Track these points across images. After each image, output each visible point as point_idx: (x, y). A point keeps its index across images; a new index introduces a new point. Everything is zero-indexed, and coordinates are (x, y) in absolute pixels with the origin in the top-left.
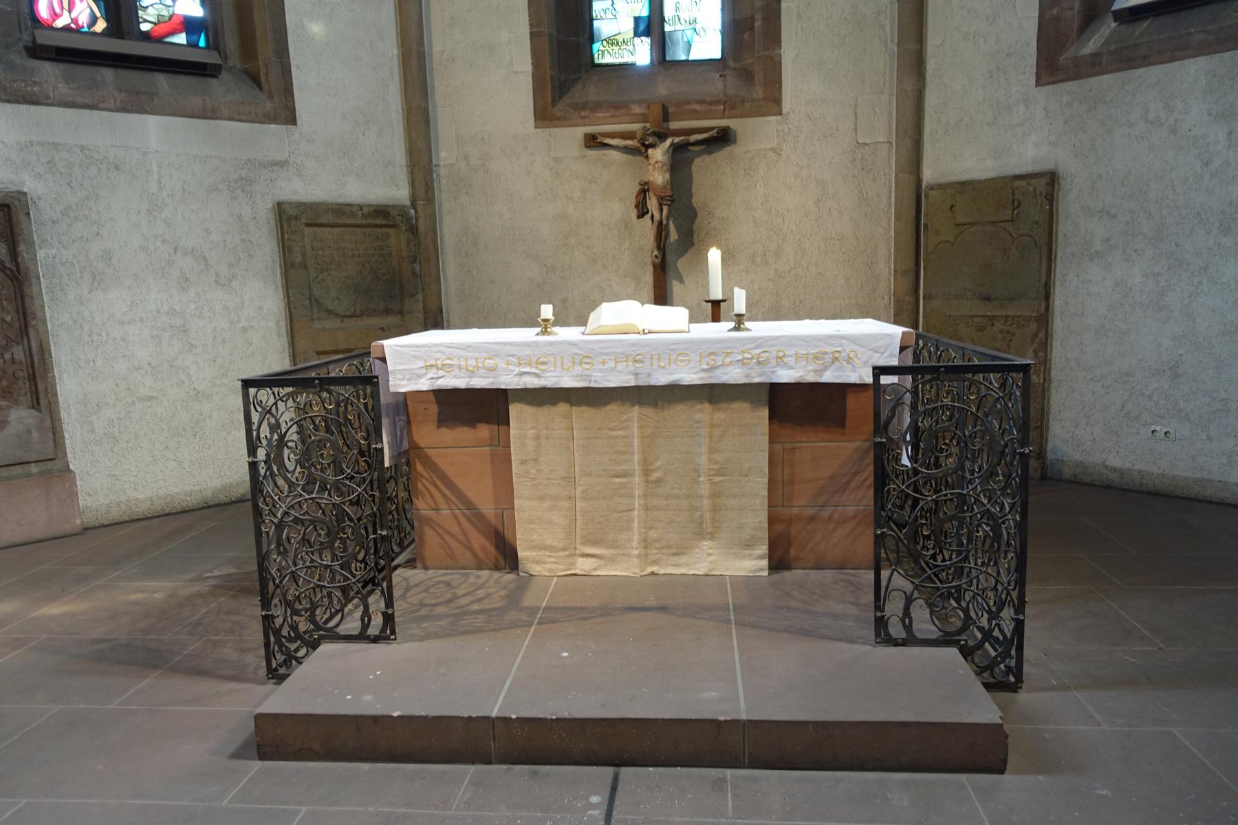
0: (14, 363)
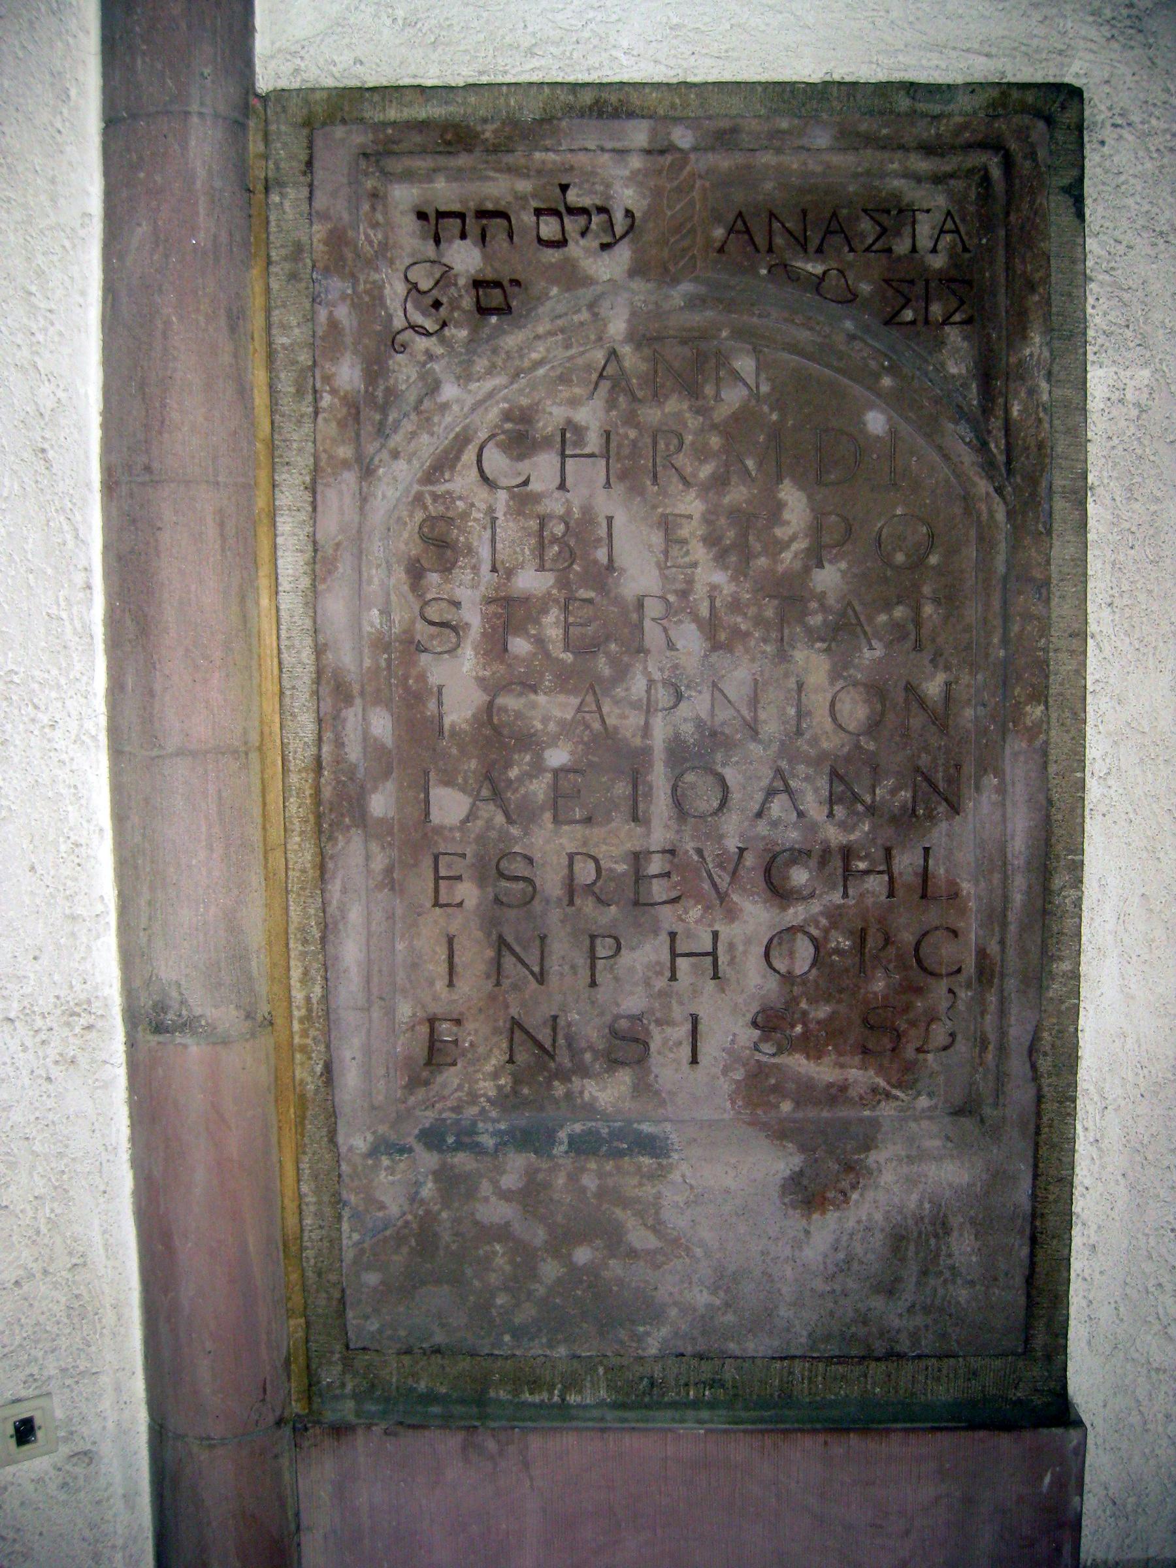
0: (924, 896)
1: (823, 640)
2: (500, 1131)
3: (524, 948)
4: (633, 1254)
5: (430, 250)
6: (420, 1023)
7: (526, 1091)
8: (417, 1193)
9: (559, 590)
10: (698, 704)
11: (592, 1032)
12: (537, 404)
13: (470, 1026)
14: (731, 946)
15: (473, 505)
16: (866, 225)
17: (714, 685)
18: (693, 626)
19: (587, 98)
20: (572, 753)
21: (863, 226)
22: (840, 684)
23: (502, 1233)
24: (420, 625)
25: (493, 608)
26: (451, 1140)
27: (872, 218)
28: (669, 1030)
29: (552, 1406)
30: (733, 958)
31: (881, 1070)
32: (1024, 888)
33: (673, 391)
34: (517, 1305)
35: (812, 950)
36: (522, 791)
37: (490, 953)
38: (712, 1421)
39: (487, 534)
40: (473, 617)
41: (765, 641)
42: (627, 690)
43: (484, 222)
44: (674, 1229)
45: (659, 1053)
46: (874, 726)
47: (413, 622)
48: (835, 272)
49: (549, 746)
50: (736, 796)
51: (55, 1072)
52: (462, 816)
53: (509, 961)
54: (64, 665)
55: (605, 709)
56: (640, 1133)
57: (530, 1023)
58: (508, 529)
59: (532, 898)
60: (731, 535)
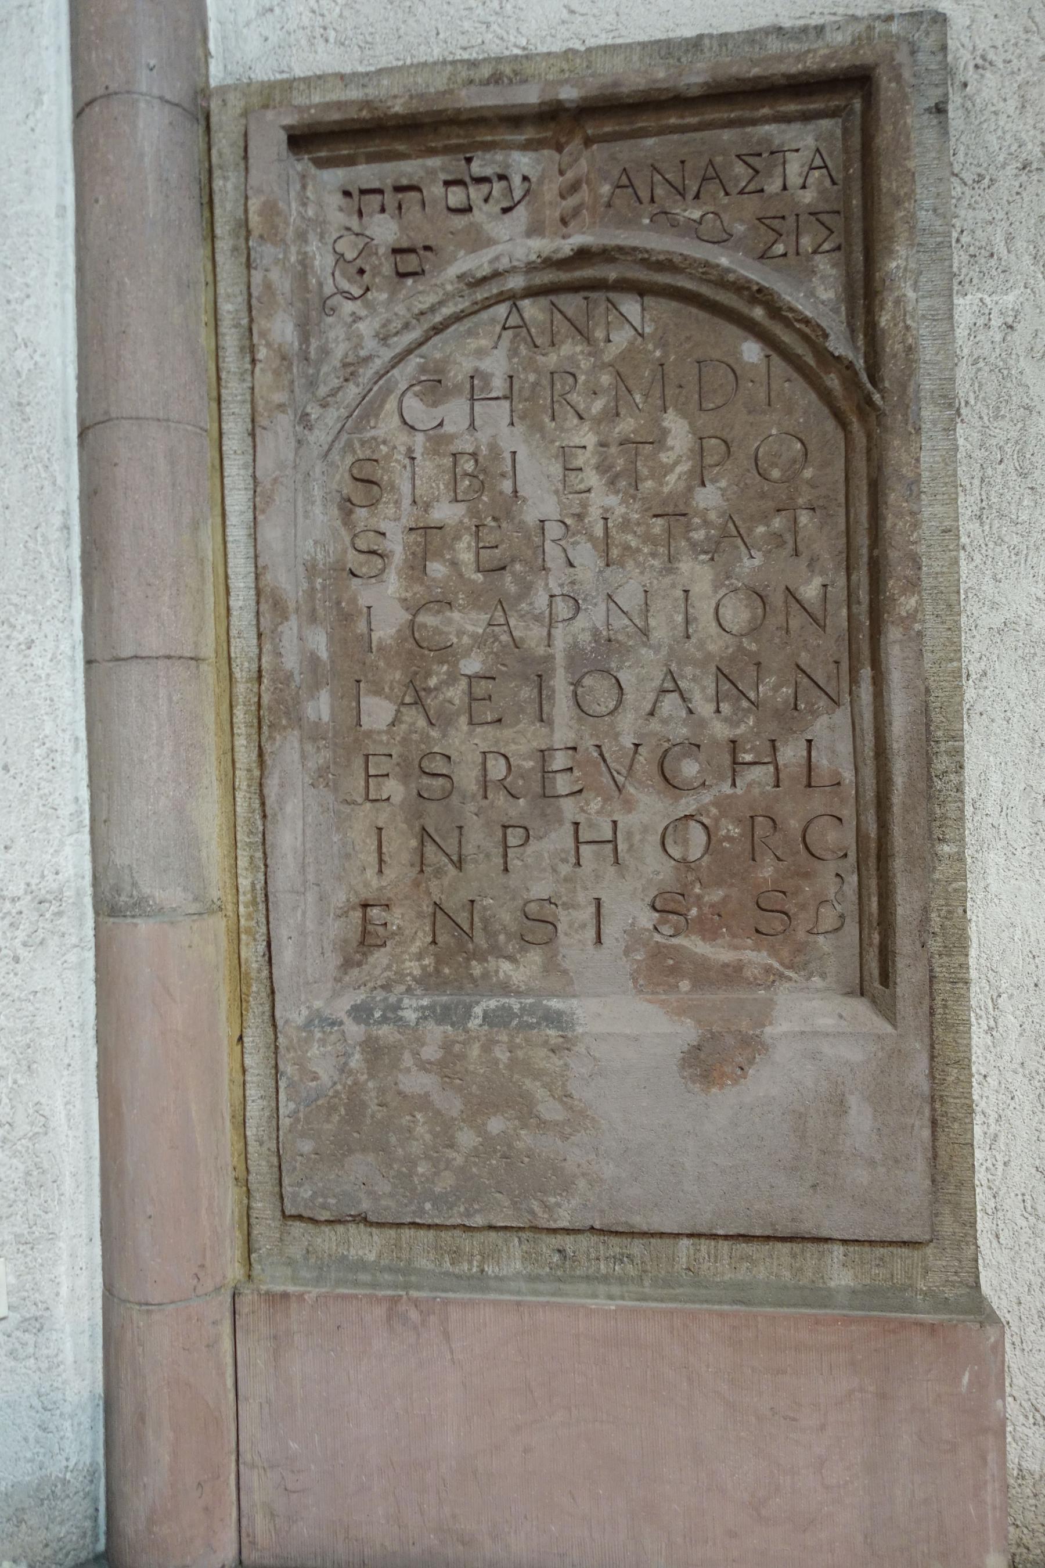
1: (706, 552)
2: (422, 1007)
3: (444, 839)
4: (543, 1125)
5: (354, 223)
6: (353, 908)
7: (447, 971)
8: (346, 1064)
9: (470, 519)
10: (595, 615)
11: (507, 917)
12: (449, 357)
13: (397, 911)
14: (629, 835)
15: (395, 447)
16: (739, 169)
17: (609, 596)
18: (589, 545)
19: (486, 72)
20: (483, 662)
21: (737, 170)
22: (722, 592)
23: (424, 1102)
24: (351, 554)
25: (413, 537)
26: (377, 1014)
27: (745, 162)
28: (574, 913)
29: (470, 1278)
30: (631, 846)
31: (773, 952)
32: (905, 770)
33: (567, 337)
34: (436, 1174)
35: (704, 838)
36: (441, 697)
37: (414, 843)
38: (623, 1298)
39: (407, 474)
40: (397, 545)
41: (654, 555)
42: (531, 604)
43: (400, 196)
44: (580, 1100)
45: (566, 934)
46: (754, 630)
47: (345, 551)
48: (711, 216)
49: (464, 657)
50: (629, 697)
51: (22, 952)
52: (390, 720)
53: (430, 849)
54: (41, 593)
55: (512, 622)
56: (548, 1009)
57: (450, 905)
58: (426, 466)
59: (451, 793)
60: (620, 463)
